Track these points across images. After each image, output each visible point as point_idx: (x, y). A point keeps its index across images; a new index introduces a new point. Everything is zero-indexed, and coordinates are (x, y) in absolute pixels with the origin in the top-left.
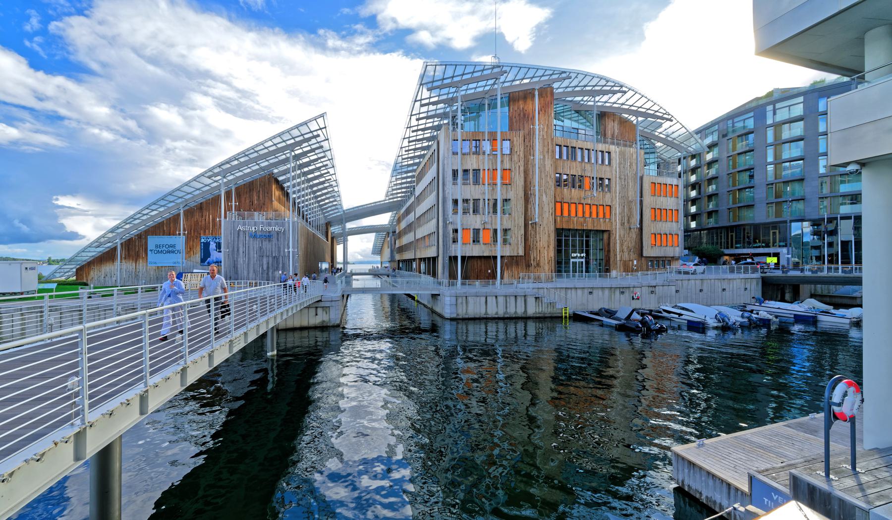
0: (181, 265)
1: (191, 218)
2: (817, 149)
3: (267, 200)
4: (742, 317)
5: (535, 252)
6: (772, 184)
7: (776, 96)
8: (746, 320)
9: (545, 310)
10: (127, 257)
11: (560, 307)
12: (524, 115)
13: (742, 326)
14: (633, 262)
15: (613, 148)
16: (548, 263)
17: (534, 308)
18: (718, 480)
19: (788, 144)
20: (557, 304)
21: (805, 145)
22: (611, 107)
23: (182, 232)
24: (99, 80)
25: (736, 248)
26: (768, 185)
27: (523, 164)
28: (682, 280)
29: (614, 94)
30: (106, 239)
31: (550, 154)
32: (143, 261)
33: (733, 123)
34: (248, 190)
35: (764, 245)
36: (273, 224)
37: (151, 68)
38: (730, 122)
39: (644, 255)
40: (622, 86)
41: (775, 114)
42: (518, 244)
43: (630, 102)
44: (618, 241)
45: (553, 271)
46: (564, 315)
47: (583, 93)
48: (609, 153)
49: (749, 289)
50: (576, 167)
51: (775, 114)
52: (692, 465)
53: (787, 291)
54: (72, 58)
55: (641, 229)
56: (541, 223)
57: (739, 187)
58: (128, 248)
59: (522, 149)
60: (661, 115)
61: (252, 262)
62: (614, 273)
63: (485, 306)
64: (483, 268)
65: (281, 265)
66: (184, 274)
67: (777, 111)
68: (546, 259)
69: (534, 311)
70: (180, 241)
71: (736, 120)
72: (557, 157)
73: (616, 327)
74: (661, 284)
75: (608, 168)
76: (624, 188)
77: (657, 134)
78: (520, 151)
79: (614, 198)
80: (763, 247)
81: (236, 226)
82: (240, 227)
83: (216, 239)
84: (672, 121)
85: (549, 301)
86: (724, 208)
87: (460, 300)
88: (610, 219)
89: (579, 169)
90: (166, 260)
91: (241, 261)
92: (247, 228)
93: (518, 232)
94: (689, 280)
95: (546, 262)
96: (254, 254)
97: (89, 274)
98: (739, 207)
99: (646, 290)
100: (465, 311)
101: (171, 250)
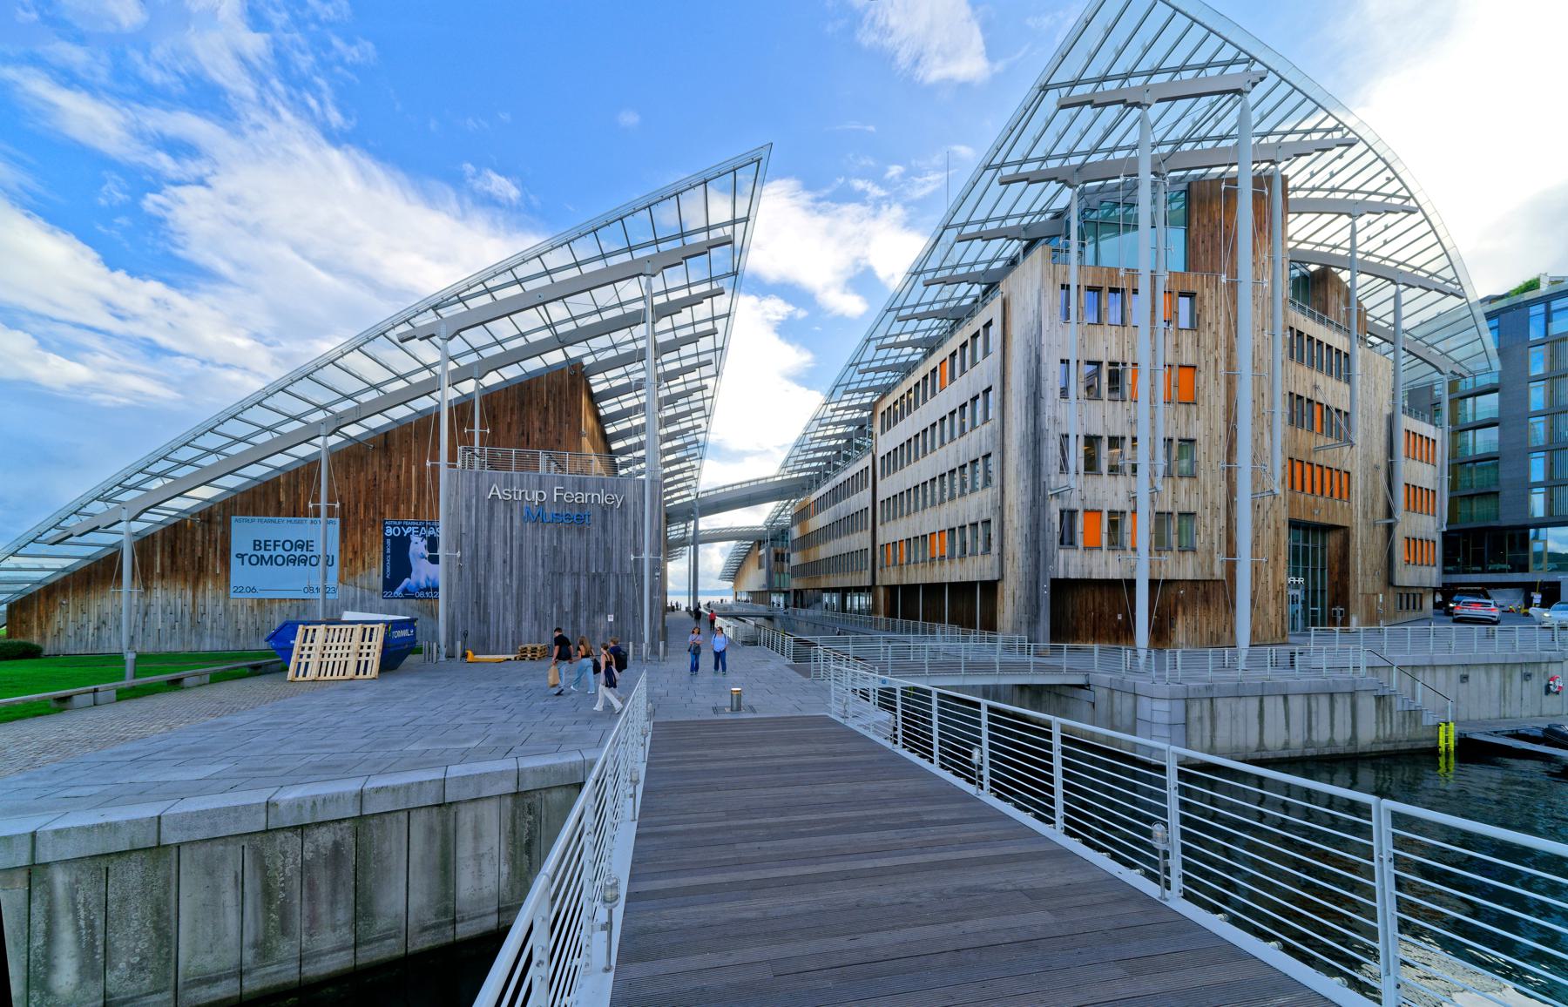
0: (320, 596)
1: (358, 472)
9: (1398, 732)
10: (168, 573)
14: (1378, 598)
16: (1276, 598)
17: (1374, 726)
20: (1425, 716)
23: (323, 504)
24: (232, 290)
34: (517, 403)
37: (324, 278)
42: (1211, 552)
54: (180, 253)
58: (173, 548)
61: (530, 591)
64: (1106, 609)
65: (612, 599)
67: (1555, 316)
68: (1270, 588)
69: (1373, 736)
70: (323, 533)
81: (484, 486)
87: (1195, 711)
91: (496, 585)
92: (517, 493)
93: (1212, 520)
95: (1271, 596)
96: (536, 565)
97: (48, 621)
101: (299, 554)
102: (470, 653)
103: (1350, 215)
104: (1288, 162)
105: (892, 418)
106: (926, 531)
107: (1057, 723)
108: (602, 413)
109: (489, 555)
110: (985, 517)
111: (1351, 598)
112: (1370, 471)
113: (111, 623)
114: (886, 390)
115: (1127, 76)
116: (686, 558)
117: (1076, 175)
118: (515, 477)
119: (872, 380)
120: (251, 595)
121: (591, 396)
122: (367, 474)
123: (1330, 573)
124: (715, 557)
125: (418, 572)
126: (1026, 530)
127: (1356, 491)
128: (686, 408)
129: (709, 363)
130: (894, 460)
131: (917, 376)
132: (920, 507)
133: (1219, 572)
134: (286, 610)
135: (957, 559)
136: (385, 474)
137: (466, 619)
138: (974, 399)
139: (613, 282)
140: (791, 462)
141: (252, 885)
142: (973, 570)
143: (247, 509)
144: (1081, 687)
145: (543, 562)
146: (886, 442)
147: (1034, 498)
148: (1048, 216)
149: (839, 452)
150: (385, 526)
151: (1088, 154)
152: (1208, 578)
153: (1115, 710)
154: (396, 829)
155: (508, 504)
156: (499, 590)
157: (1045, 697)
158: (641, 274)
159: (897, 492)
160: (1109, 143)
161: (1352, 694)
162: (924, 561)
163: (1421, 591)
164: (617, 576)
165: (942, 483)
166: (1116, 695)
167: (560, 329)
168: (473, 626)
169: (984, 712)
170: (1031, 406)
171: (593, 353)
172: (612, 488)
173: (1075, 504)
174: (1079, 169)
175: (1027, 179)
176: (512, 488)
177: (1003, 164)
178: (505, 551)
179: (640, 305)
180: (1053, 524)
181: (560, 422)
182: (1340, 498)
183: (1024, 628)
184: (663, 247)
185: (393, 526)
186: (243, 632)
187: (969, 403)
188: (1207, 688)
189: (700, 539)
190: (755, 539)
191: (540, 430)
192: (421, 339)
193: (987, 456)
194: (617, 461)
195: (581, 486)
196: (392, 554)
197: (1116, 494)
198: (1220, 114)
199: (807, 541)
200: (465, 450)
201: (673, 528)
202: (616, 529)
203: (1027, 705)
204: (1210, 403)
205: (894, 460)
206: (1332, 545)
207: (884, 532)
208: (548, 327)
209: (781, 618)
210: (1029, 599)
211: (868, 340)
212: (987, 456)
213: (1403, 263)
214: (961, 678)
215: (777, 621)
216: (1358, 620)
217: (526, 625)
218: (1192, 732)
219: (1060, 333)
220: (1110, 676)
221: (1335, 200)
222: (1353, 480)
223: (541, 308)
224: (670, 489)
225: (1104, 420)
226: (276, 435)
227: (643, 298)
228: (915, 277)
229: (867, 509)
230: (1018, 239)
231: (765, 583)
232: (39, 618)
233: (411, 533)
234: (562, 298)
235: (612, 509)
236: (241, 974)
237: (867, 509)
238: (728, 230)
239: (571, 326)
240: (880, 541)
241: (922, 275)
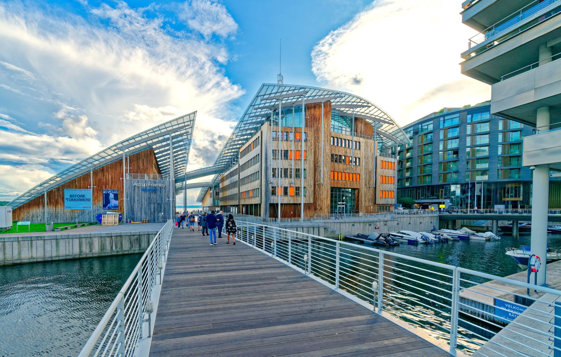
2: (466, 144)
3: (149, 166)
4: (435, 237)
6: (442, 163)
7: (445, 112)
8: (437, 239)
11: (338, 234)
12: (314, 118)
13: (436, 243)
14: (371, 208)
15: (361, 140)
16: (327, 208)
18: (477, 303)
19: (451, 140)
21: (460, 142)
22: (360, 115)
25: (422, 199)
26: (439, 163)
27: (313, 148)
28: (400, 218)
29: (363, 107)
30: (35, 191)
31: (328, 142)
32: (61, 206)
33: (422, 126)
34: (136, 159)
35: (436, 197)
36: (157, 182)
38: (420, 126)
39: (377, 203)
40: (368, 103)
41: (444, 122)
43: (371, 113)
44: (363, 195)
45: (330, 213)
46: (340, 238)
47: (346, 106)
48: (359, 143)
49: (433, 222)
50: (342, 151)
51: (444, 122)
52: (463, 299)
53: (450, 223)
55: (375, 188)
56: (323, 184)
57: (424, 164)
58: (50, 197)
59: (313, 139)
60: (388, 121)
62: (361, 214)
64: (288, 211)
65: (163, 209)
66: (103, 215)
67: (446, 121)
68: (326, 205)
70: (89, 193)
71: (423, 125)
72: (332, 144)
73: (372, 244)
74: (390, 220)
75: (358, 152)
76: (367, 163)
77: (380, 130)
78: (312, 140)
79: (361, 170)
80: (436, 199)
82: (136, 184)
83: (114, 191)
84: (393, 125)
85: (332, 230)
86: (415, 176)
88: (359, 182)
89: (343, 152)
90: (79, 206)
91: (136, 206)
93: (310, 189)
94: (404, 218)
97: (20, 216)
98: (424, 176)
99: (382, 223)
100: (71, 250)
101: (82, 198)
110: (258, 187)
113: (35, 216)
120: (70, 209)
122: (98, 178)
124: (194, 194)
125: (112, 203)
127: (362, 179)
133: (312, 201)
134: (79, 212)
138: (257, 155)
141: (129, 241)
143: (68, 187)
146: (242, 161)
154: (143, 236)
155: (138, 187)
161: (319, 227)
163: (390, 205)
186: (68, 218)
190: (208, 188)
193: (259, 171)
194: (156, 156)
196: (105, 198)
199: (224, 189)
201: (178, 184)
202: (163, 193)
221: (349, 105)
226: (80, 170)
231: (212, 203)
232: (18, 215)
236: (128, 251)
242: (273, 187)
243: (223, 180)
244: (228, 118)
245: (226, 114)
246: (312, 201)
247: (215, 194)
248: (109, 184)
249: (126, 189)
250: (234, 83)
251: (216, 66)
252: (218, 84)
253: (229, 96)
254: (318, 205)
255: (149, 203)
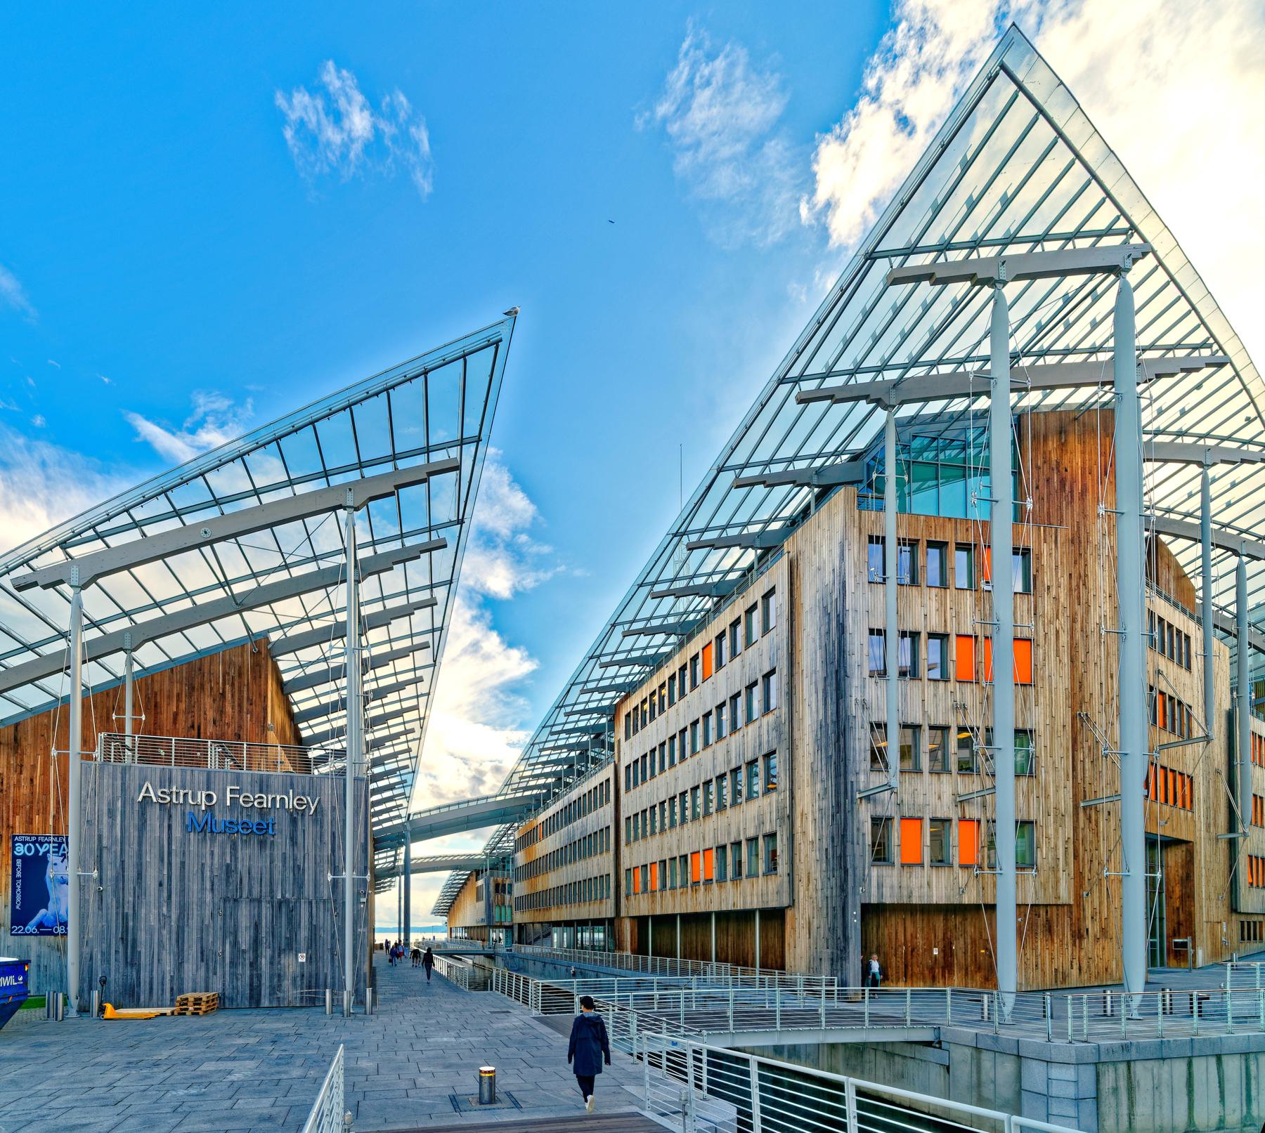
5: (1096, 894)
12: (1062, 482)
34: (185, 688)
36: (276, 784)
42: (1055, 869)
59: (1064, 581)
61: (194, 923)
63: (1186, 1099)
64: (920, 942)
65: (304, 933)
81: (133, 783)
87: (1108, 1081)
91: (149, 915)
93: (1056, 831)
96: (203, 889)
102: (109, 1006)
103: (1200, 464)
104: (1146, 385)
105: (638, 721)
106: (686, 850)
107: (851, 1083)
108: (295, 709)
109: (140, 875)
110: (768, 829)
111: (1197, 928)
112: (1211, 776)
114: (629, 689)
115: (975, 244)
116: (395, 891)
117: (893, 392)
118: (174, 773)
119: (577, 722)
121: (281, 685)
123: (1169, 897)
126: (826, 843)
128: (397, 707)
129: (424, 646)
130: (641, 770)
131: (673, 667)
132: (657, 830)
133: (1065, 894)
135: (729, 883)
136: (14, 777)
137: (109, 962)
139: (302, 517)
140: (516, 779)
142: (752, 895)
144: (928, 1044)
145: (213, 885)
146: (630, 750)
147: (838, 804)
148: (845, 457)
149: (571, 766)
150: (14, 843)
151: (906, 367)
152: (1053, 902)
153: (984, 1078)
156: (153, 921)
157: (869, 1056)
158: (340, 507)
159: (647, 805)
160: (931, 355)
162: (684, 885)
164: (310, 903)
165: (707, 793)
166: (987, 1059)
167: (238, 588)
168: (117, 970)
169: (850, 1096)
170: (832, 690)
171: (281, 627)
172: (303, 788)
173: (892, 811)
174: (896, 384)
175: (830, 397)
176: (170, 787)
177: (801, 378)
178: (160, 871)
179: (341, 559)
180: (864, 834)
181: (240, 711)
182: (1184, 806)
183: (826, 966)
184: (369, 472)
185: (24, 843)
187: (701, 720)
188: (1125, 1048)
189: (412, 868)
190: (471, 869)
191: (214, 723)
192: (45, 587)
193: (769, 755)
195: (263, 785)
197: (939, 798)
198: (1072, 318)
199: (533, 869)
200: (107, 742)
202: (309, 842)
203: (841, 1066)
204: (1050, 685)
205: (641, 770)
206: (1171, 863)
207: (631, 853)
208: (221, 585)
209: (503, 956)
210: (832, 930)
211: (614, 625)
212: (769, 755)
213: (1246, 531)
214: (776, 1035)
215: (499, 959)
216: (1204, 953)
217: (189, 968)
218: (1104, 1109)
219: (868, 594)
220: (975, 1031)
222: (1195, 786)
223: (207, 550)
224: (377, 808)
225: (923, 705)
227: (345, 551)
228: (676, 539)
229: (608, 828)
230: (808, 485)
231: (484, 916)
233: (48, 851)
234: (235, 536)
235: (303, 815)
237: (608, 828)
238: (454, 452)
239: (251, 585)
240: (626, 863)
241: (685, 537)
242: (876, 821)
243: (527, 840)
244: (498, 724)
245: (495, 712)
246: (1065, 894)
247: (492, 888)
248: (45, 811)
249: (87, 822)
250: (511, 644)
251: (470, 607)
252: (475, 647)
253: (501, 674)
254: (1088, 913)
255: (226, 900)
